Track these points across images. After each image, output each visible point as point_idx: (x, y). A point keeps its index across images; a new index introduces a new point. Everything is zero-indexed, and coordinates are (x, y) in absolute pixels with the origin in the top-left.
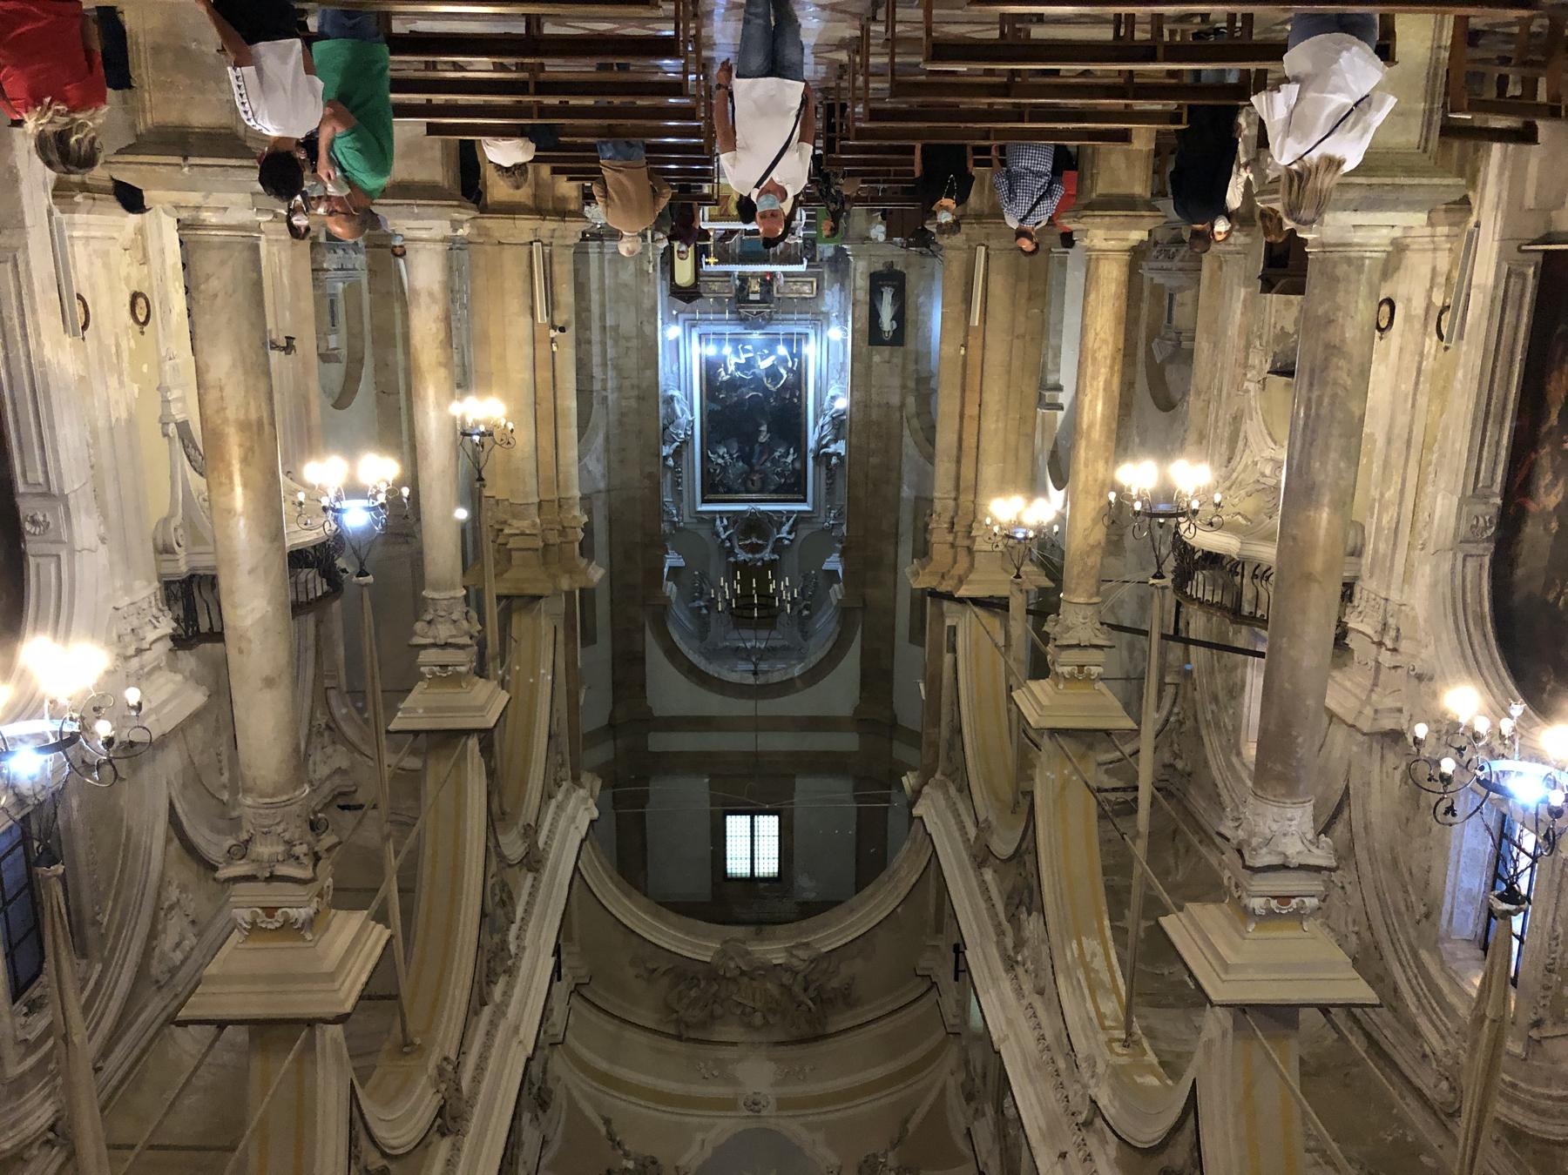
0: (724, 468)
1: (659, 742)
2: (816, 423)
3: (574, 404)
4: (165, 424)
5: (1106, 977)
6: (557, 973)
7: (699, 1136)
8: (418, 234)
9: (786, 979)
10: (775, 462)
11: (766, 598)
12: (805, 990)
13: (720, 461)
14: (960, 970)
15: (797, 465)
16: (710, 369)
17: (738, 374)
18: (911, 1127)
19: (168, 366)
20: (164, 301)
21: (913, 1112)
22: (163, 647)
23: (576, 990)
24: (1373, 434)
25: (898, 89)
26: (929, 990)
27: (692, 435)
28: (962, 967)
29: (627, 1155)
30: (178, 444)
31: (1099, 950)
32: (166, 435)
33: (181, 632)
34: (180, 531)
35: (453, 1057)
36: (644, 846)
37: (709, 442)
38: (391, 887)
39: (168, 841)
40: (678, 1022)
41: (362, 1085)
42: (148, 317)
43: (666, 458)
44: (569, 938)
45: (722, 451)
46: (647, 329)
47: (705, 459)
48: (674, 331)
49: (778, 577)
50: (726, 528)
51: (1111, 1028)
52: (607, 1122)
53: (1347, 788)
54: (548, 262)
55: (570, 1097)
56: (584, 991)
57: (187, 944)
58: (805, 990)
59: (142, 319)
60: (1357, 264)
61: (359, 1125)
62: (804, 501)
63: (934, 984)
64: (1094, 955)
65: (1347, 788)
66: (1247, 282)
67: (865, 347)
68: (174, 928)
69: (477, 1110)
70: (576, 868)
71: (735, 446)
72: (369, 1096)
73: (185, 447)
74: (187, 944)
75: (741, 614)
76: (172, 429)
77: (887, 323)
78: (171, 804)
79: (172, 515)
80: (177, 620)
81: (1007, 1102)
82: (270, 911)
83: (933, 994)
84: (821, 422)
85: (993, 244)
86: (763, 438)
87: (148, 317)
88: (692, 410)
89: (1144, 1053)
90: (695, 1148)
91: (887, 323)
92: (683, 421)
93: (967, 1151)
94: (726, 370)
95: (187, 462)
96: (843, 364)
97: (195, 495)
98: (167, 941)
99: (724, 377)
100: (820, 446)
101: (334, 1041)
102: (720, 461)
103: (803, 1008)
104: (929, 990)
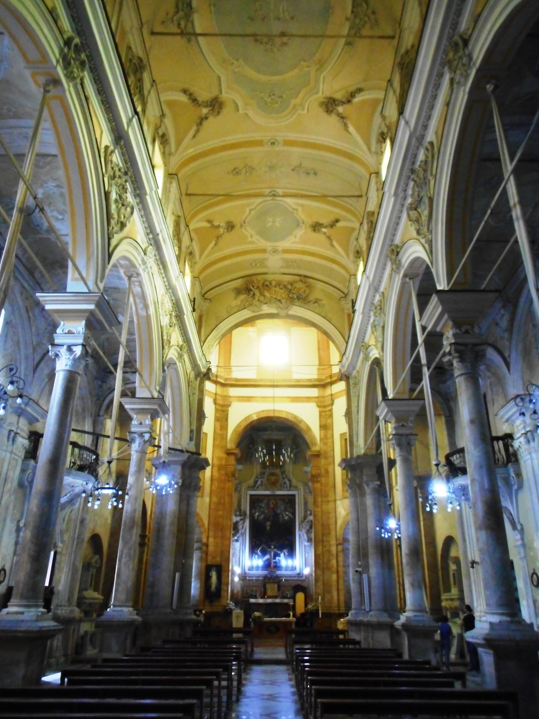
0: (286, 510)
1: (314, 392)
2: (245, 530)
3: (309, 257)
4: (522, 529)
5: (138, 301)
6: (354, 303)
7: (297, 240)
8: (152, 299)
9: (262, 298)
10: (263, 512)
11: (269, 453)
12: (254, 294)
13: (287, 513)
14: (193, 302)
15: (254, 511)
16: (291, 553)
17: (279, 552)
18: (214, 242)
19: (523, 555)
20: (526, 584)
21: (213, 248)
22: (516, 436)
23: (346, 295)
24: (12, 523)
25: (211, 681)
26: (205, 294)
27: (299, 524)
28: (192, 303)
29: (325, 233)
30: (516, 520)
31: (140, 311)
32: (521, 525)
33: (510, 441)
34: (513, 483)
35: (393, 273)
36: (319, 349)
37: (292, 521)
38: (420, 339)
39: (509, 356)
40: (306, 283)
41: (428, 265)
42: (532, 576)
43: (311, 514)
44: (349, 316)
45: (286, 518)
46: (319, 572)
47: (294, 514)
48: (307, 571)
49: (264, 463)
50: (285, 483)
51: (137, 281)
52: (333, 246)
53: (34, 374)
54: (362, 602)
55: (348, 255)
56: (343, 295)
57: (499, 316)
58: (254, 294)
59: (535, 576)
60: (23, 597)
61: (428, 251)
62: (251, 495)
63: (203, 296)
64: (142, 309)
65: (34, 374)
66: (59, 592)
67: (224, 564)
68: (504, 323)
69: (384, 253)
70: (347, 343)
71: (281, 520)
72: (424, 261)
73: (513, 519)
74: (499, 316)
75: (280, 445)
76: (519, 527)
77: (214, 576)
78: (509, 370)
79: (517, 491)
80: (512, 446)
81: (177, 253)
82: (467, 332)
83: (203, 292)
84: (243, 530)
85: (169, 610)
86: (268, 523)
87: (532, 576)
88: (300, 536)
89: (125, 273)
90: (298, 236)
91: (214, 576)
92: (304, 531)
93: (193, 234)
94: (284, 554)
95: (512, 513)
96: (233, 556)
97: (509, 500)
98: (506, 318)
99: (286, 551)
100: (244, 520)
101: (439, 283)
102: (287, 513)
103: (255, 287)
104: (205, 294)
